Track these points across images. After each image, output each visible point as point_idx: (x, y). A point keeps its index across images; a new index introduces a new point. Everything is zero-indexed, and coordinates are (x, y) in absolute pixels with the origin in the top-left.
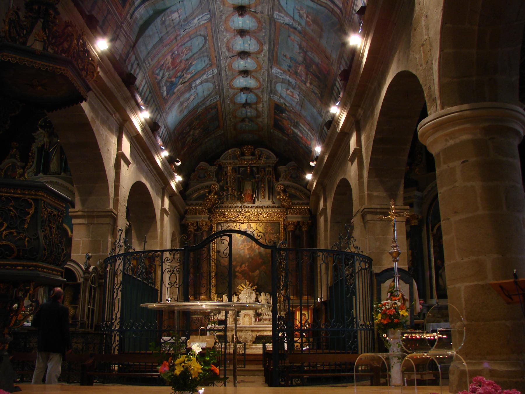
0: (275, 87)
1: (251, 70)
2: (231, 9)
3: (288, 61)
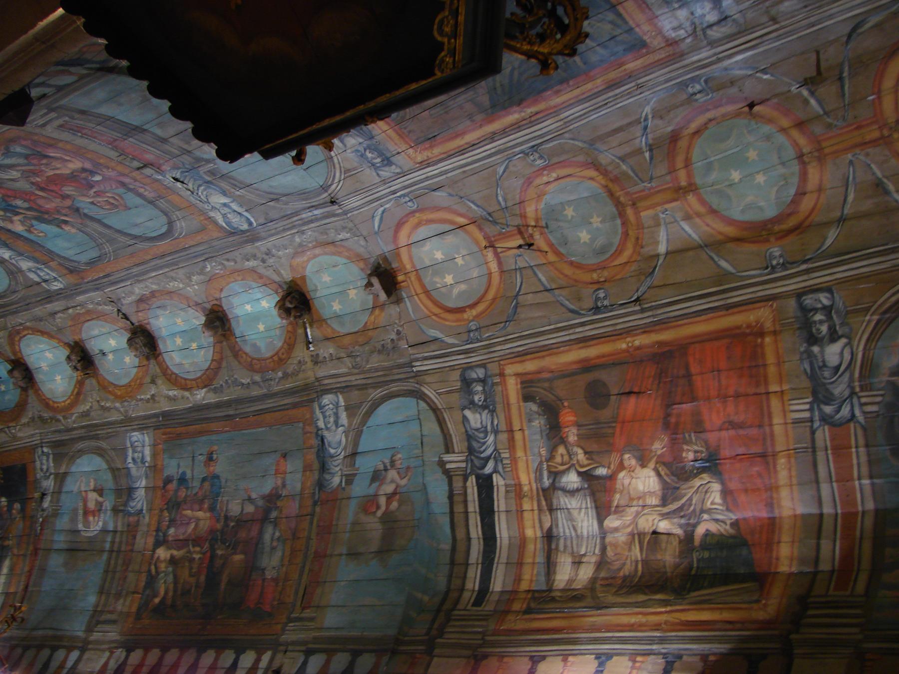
0: (81, 452)
1: (101, 372)
2: (288, 276)
3: (200, 471)
